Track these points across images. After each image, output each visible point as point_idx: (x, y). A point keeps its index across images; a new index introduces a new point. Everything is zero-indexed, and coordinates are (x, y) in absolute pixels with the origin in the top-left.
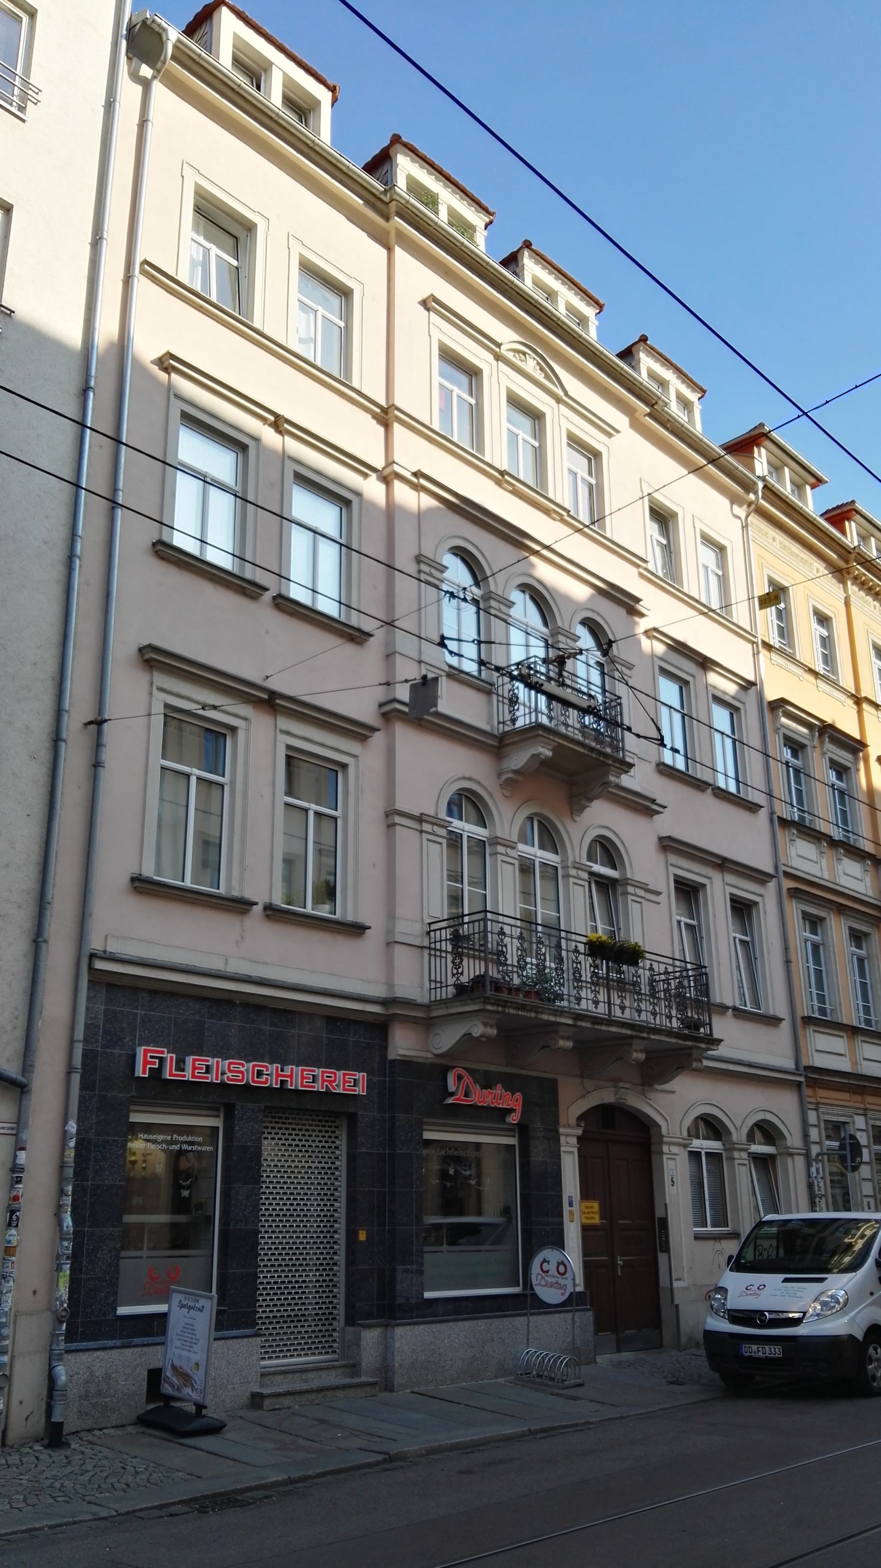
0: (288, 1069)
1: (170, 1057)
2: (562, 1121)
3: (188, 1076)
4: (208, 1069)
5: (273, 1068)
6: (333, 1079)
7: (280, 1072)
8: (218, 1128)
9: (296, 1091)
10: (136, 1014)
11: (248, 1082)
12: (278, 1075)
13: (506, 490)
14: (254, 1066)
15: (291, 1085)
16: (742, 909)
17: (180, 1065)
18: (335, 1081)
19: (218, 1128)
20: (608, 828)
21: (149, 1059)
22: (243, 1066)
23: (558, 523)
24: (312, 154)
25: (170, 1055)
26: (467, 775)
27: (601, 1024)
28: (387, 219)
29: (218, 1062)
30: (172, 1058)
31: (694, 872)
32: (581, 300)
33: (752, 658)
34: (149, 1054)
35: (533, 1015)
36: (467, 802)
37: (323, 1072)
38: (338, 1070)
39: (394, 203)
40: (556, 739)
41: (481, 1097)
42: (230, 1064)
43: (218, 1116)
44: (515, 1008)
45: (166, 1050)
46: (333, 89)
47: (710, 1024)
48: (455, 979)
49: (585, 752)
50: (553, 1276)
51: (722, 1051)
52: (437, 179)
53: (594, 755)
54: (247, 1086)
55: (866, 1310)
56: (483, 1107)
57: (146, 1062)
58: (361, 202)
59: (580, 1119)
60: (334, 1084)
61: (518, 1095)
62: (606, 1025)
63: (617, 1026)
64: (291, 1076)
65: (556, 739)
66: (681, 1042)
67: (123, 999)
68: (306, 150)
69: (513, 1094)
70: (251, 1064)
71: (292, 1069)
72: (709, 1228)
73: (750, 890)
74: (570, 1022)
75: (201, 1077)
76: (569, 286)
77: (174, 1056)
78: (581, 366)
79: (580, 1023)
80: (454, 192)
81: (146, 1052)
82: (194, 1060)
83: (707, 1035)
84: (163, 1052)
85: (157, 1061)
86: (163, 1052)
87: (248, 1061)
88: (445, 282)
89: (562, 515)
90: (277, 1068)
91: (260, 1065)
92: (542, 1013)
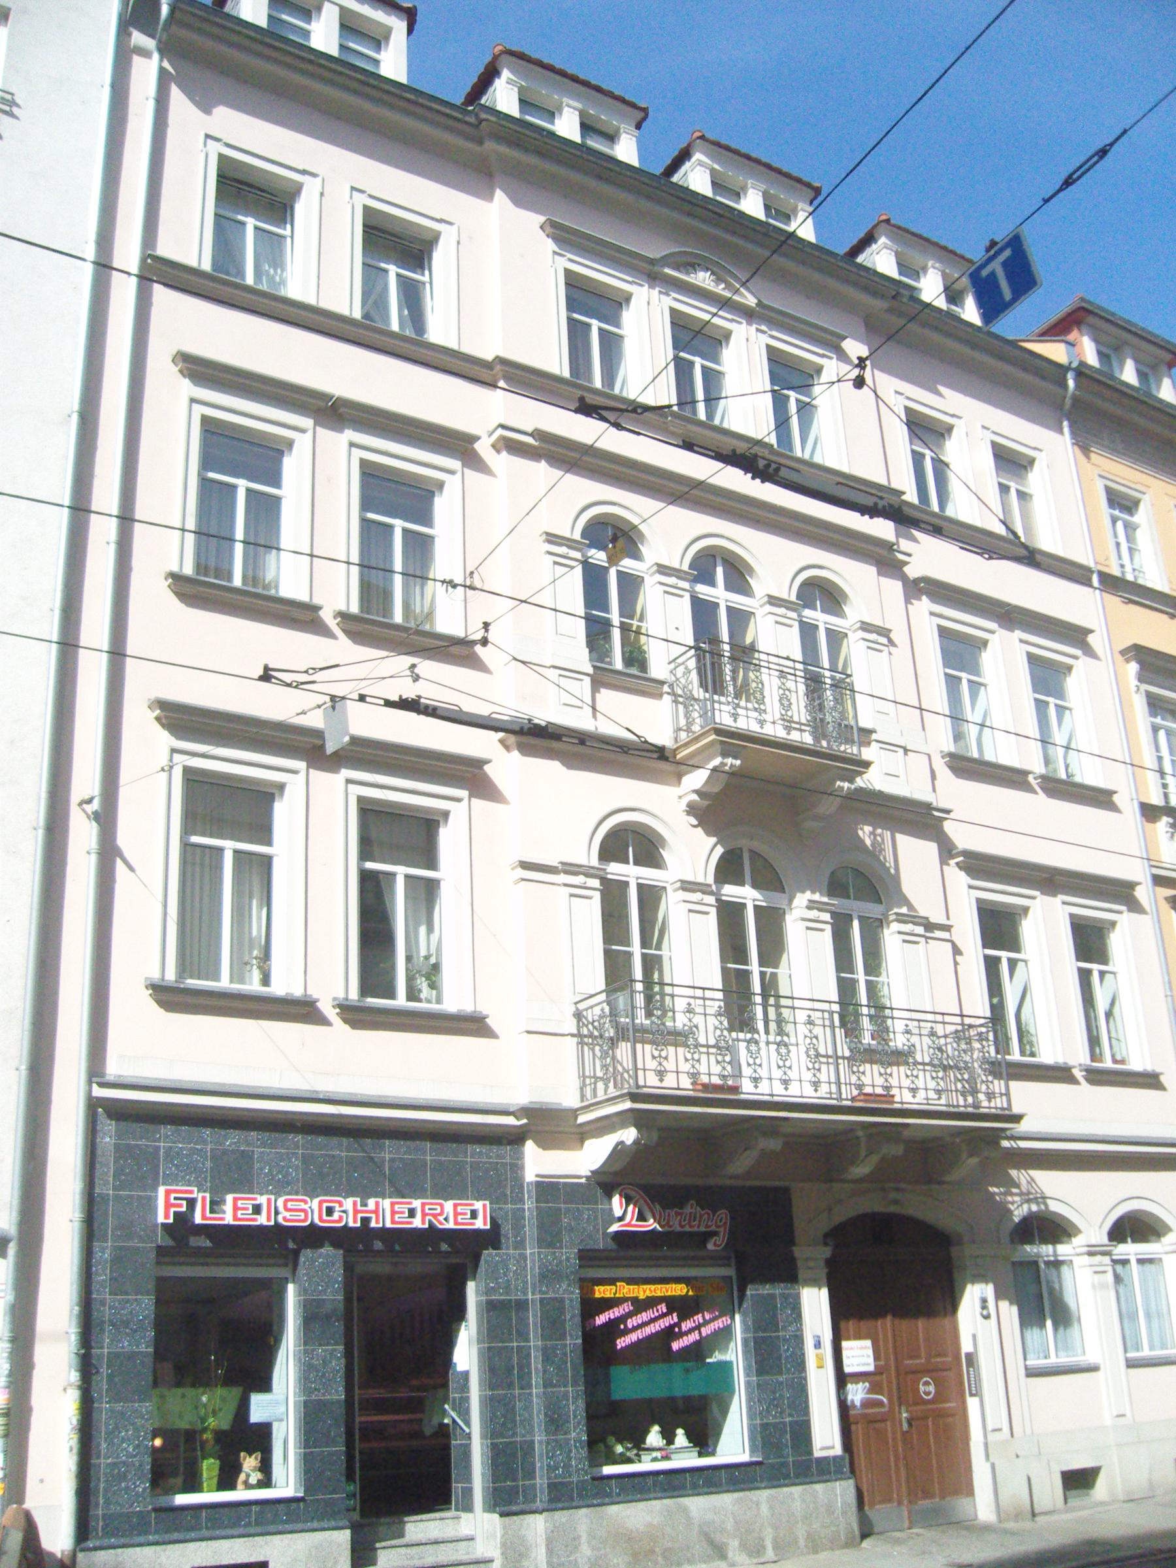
0: (371, 1203)
1: (202, 1197)
3: (229, 1219)
4: (412, 1213)
5: (348, 1203)
6: (439, 1211)
7: (359, 1207)
9: (384, 1230)
10: (159, 1147)
11: (312, 1223)
12: (356, 1212)
14: (321, 1203)
15: (377, 1222)
16: (1090, 942)
17: (216, 1205)
18: (441, 1213)
19: (731, 1278)
21: (172, 1201)
22: (305, 1202)
25: (200, 1195)
28: (480, 142)
29: (269, 1200)
30: (204, 1198)
31: (1002, 894)
33: (624, 433)
34: (173, 1195)
37: (423, 1205)
38: (446, 1200)
39: (484, 123)
42: (286, 1201)
43: (729, 1265)
45: (196, 1189)
46: (411, 16)
47: (1008, 1094)
51: (1024, 1127)
57: (168, 1205)
60: (441, 1218)
64: (376, 1212)
67: (134, 1124)
69: (714, 1212)
70: (316, 1201)
71: (377, 1204)
75: (246, 1218)
77: (208, 1195)
81: (168, 1193)
82: (235, 1200)
83: (1003, 1109)
84: (191, 1192)
85: (184, 1203)
86: (191, 1192)
87: (312, 1197)
90: (355, 1204)
91: (330, 1200)
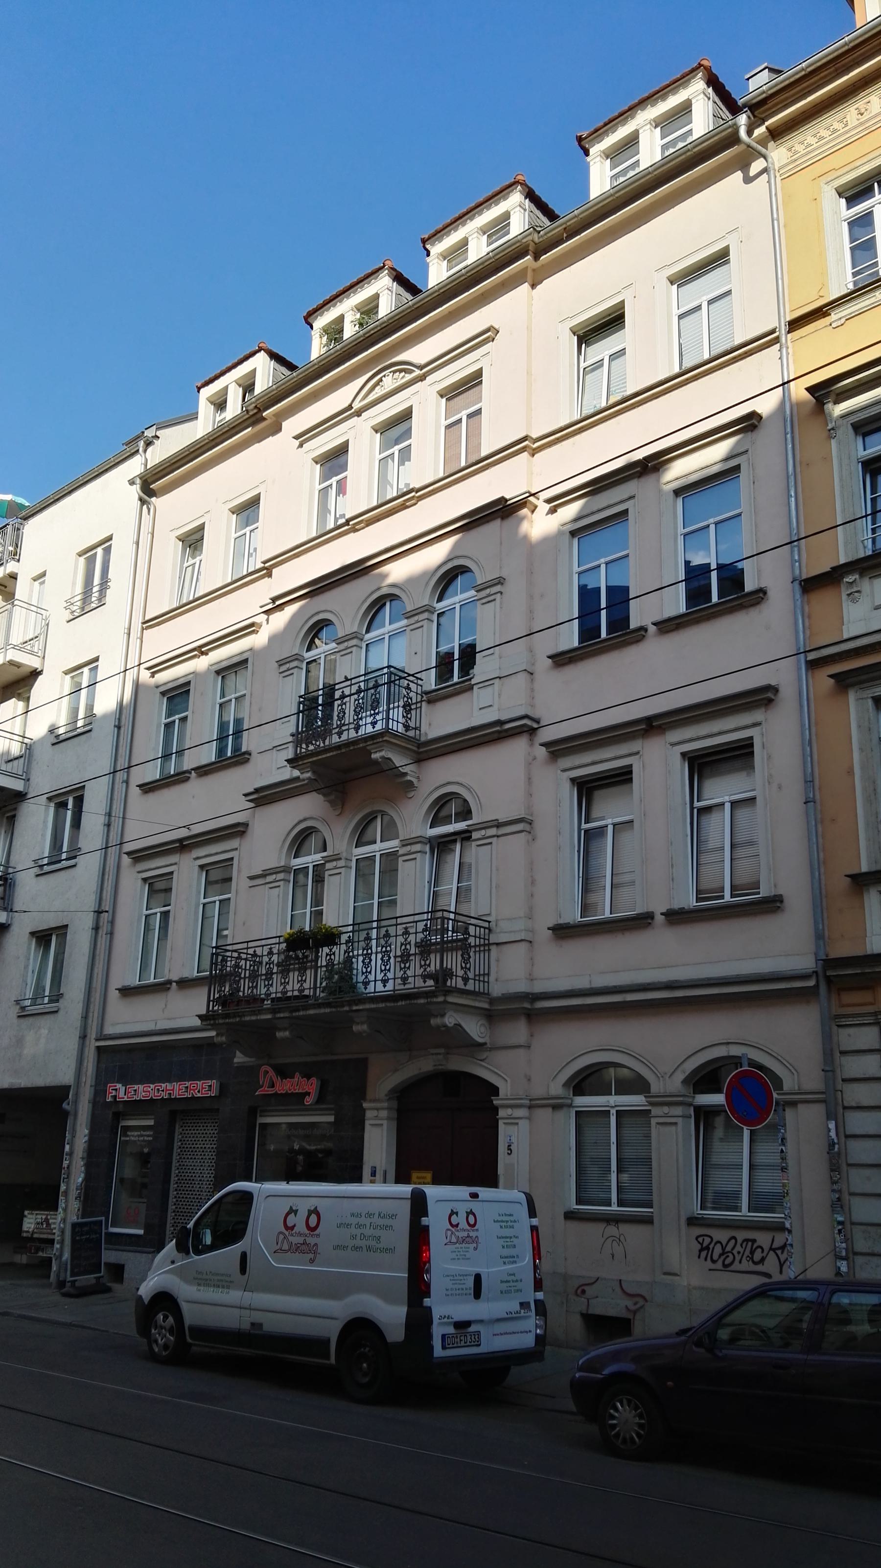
2: (370, 1094)
8: (576, 1112)
9: (175, 1098)
13: (363, 528)
19: (576, 1112)
20: (449, 783)
23: (420, 503)
24: (237, 429)
26: (302, 818)
27: (298, 1010)
32: (463, 226)
35: (238, 1019)
36: (301, 840)
40: (305, 761)
41: (285, 1086)
44: (223, 1018)
48: (422, 970)
49: (335, 753)
50: (300, 1234)
52: (341, 301)
53: (343, 750)
54: (151, 1099)
55: (163, 1275)
56: (281, 1094)
58: (250, 429)
59: (392, 1091)
61: (314, 1080)
62: (303, 1010)
63: (315, 1008)
65: (305, 761)
66: (392, 1004)
68: (213, 443)
72: (614, 1207)
73: (726, 728)
74: (287, 1015)
76: (469, 218)
78: (446, 312)
79: (278, 1015)
80: (355, 292)
88: (297, 416)
89: (413, 497)
92: (244, 1016)
